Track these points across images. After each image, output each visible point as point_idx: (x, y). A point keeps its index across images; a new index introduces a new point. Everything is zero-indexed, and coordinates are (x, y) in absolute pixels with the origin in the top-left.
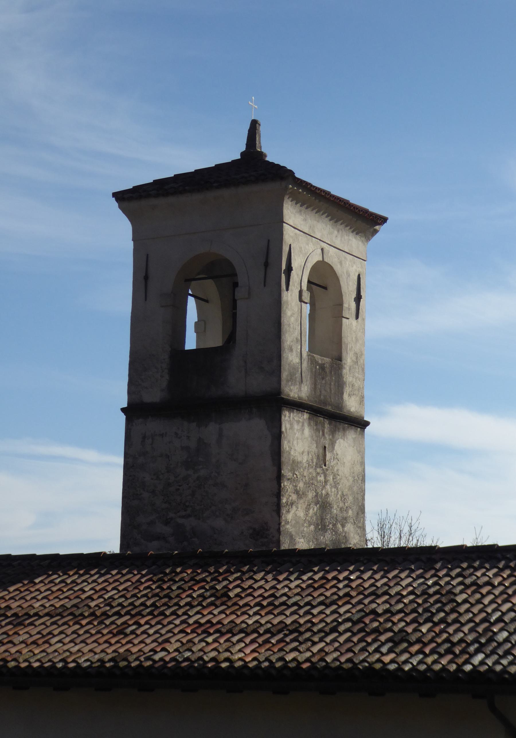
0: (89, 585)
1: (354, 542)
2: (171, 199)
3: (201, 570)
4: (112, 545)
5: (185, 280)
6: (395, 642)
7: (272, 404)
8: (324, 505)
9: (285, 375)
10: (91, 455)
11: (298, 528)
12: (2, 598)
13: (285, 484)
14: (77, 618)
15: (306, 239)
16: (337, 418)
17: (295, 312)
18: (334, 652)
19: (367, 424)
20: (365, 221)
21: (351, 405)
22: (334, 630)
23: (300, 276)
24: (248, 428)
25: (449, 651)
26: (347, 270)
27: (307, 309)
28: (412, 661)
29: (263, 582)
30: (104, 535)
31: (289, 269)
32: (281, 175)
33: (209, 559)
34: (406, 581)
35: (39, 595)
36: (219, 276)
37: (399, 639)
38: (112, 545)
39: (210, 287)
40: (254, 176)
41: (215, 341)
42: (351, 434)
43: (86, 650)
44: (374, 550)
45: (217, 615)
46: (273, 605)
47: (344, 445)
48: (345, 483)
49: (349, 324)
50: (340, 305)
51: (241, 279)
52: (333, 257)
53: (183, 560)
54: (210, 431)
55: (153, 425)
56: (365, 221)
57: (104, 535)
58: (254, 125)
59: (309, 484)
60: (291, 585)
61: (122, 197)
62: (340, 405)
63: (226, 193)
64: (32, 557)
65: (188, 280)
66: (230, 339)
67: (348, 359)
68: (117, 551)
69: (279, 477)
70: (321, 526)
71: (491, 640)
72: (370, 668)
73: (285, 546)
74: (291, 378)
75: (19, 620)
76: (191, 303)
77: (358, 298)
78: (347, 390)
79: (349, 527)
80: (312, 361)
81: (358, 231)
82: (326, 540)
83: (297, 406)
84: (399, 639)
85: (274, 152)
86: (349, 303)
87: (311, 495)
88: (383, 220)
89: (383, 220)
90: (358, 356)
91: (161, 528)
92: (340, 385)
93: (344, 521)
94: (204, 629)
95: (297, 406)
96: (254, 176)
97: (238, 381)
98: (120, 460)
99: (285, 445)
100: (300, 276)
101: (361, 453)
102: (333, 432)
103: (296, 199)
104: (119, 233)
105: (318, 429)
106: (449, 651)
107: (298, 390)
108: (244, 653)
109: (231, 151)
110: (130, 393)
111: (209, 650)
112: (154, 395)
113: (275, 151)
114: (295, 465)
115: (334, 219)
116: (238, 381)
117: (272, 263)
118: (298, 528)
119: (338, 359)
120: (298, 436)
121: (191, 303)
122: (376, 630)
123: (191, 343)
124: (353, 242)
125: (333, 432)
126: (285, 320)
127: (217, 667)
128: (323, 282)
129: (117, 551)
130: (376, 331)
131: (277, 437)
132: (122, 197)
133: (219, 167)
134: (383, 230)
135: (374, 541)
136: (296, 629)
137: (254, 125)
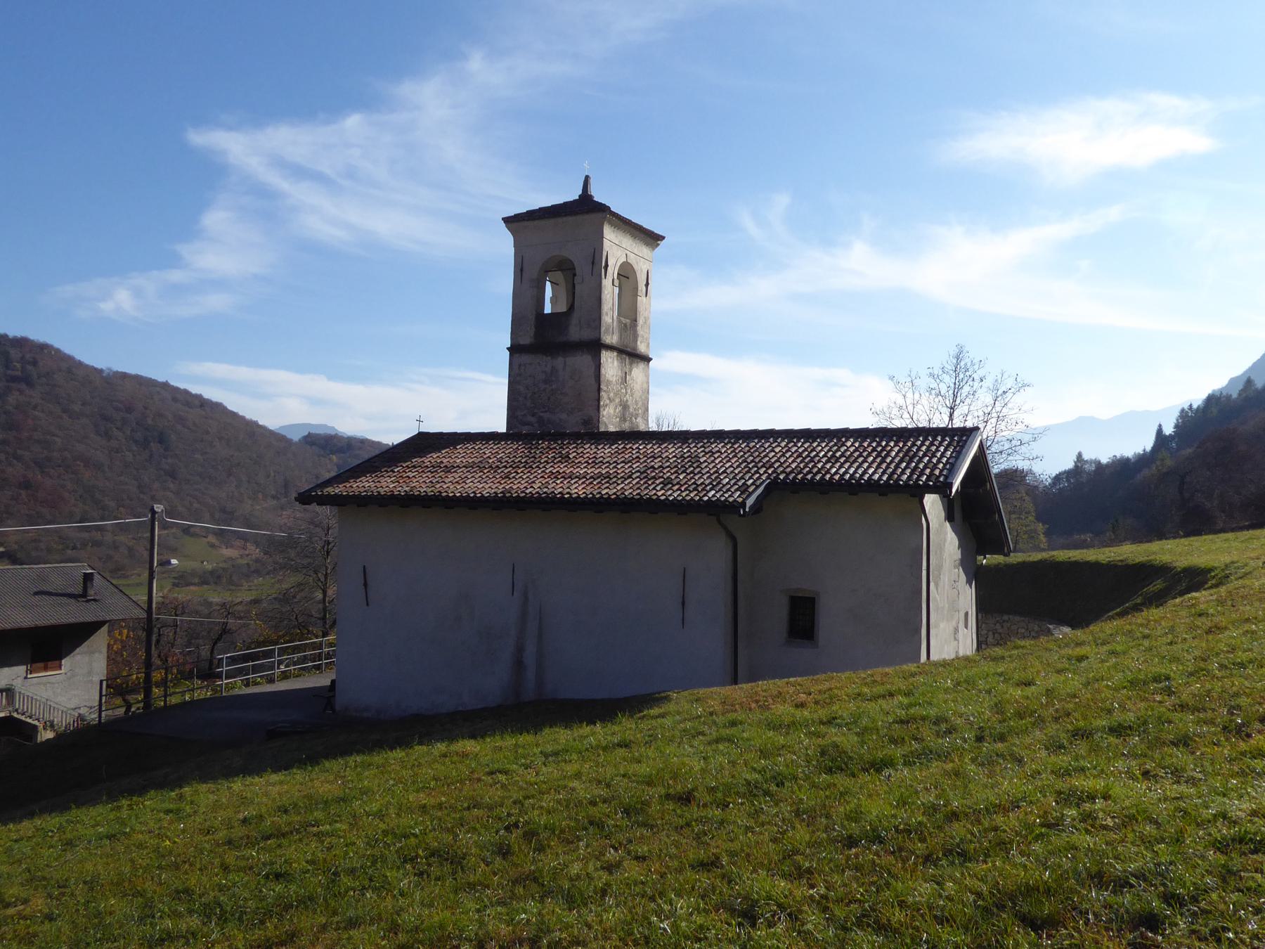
0: (488, 450)
1: (642, 428)
2: (536, 222)
3: (107, 307)
4: (502, 427)
5: (545, 271)
6: (664, 484)
7: (595, 347)
8: (625, 406)
9: (603, 329)
10: (489, 378)
11: (610, 419)
12: (5, 442)
13: (602, 393)
14: (481, 469)
15: (617, 248)
16: (633, 356)
17: (610, 292)
18: (629, 489)
19: (651, 359)
20: (652, 239)
21: (642, 348)
22: (630, 477)
23: (613, 270)
24: (581, 361)
25: (695, 489)
26: (641, 268)
27: (616, 290)
28: (674, 495)
29: (589, 450)
30: (498, 422)
31: (607, 265)
32: (602, 209)
33: (558, 436)
34: (672, 450)
35: (459, 455)
36: (564, 268)
37: (667, 483)
38: (502, 427)
39: (559, 276)
40: (586, 209)
41: (562, 308)
42: (642, 365)
43: (486, 487)
44: (654, 433)
45: (562, 468)
46: (594, 463)
47: (637, 372)
48: (637, 395)
49: (641, 300)
50: (636, 288)
51: (578, 271)
52: (632, 260)
53: (542, 437)
54: (559, 361)
55: (525, 358)
56: (652, 239)
57: (498, 422)
58: (587, 178)
59: (616, 394)
60: (605, 451)
61: (508, 221)
62: (635, 348)
63: (570, 219)
64: (441, 434)
65: (547, 272)
66: (571, 308)
67: (641, 321)
68: (504, 430)
69: (599, 390)
70: (623, 419)
71: (719, 483)
72: (650, 498)
73: (602, 429)
74: (607, 330)
75: (448, 470)
76: (548, 285)
77: (647, 284)
78: (640, 339)
79: (639, 420)
80: (620, 322)
81: (647, 244)
82: (626, 427)
83: (610, 348)
84: (667, 483)
85: (598, 195)
86: (642, 287)
87: (617, 400)
88: (663, 238)
89: (663, 238)
90: (646, 319)
91: (531, 419)
92: (635, 336)
93: (637, 416)
94: (555, 476)
95: (610, 348)
96: (586, 209)
97: (576, 332)
98: (505, 381)
99: (603, 371)
100: (613, 270)
101: (647, 376)
102: (631, 364)
103: (611, 224)
104: (504, 245)
105: (622, 362)
106: (695, 489)
107: (611, 338)
108: (578, 490)
109: (573, 194)
110: (512, 339)
111: (558, 488)
112: (526, 340)
113: (599, 194)
114: (609, 382)
115: (634, 236)
116: (576, 332)
117: (596, 261)
118: (610, 419)
119: (635, 320)
120: (610, 365)
121: (548, 285)
122: (653, 477)
123: (548, 309)
124: (644, 251)
125: (631, 364)
126: (603, 297)
127: (563, 497)
128: (626, 274)
129: (504, 430)
130: (657, 306)
131: (598, 366)
132: (508, 221)
133: (565, 204)
134: (662, 243)
135: (653, 427)
136: (608, 476)
137: (587, 178)
